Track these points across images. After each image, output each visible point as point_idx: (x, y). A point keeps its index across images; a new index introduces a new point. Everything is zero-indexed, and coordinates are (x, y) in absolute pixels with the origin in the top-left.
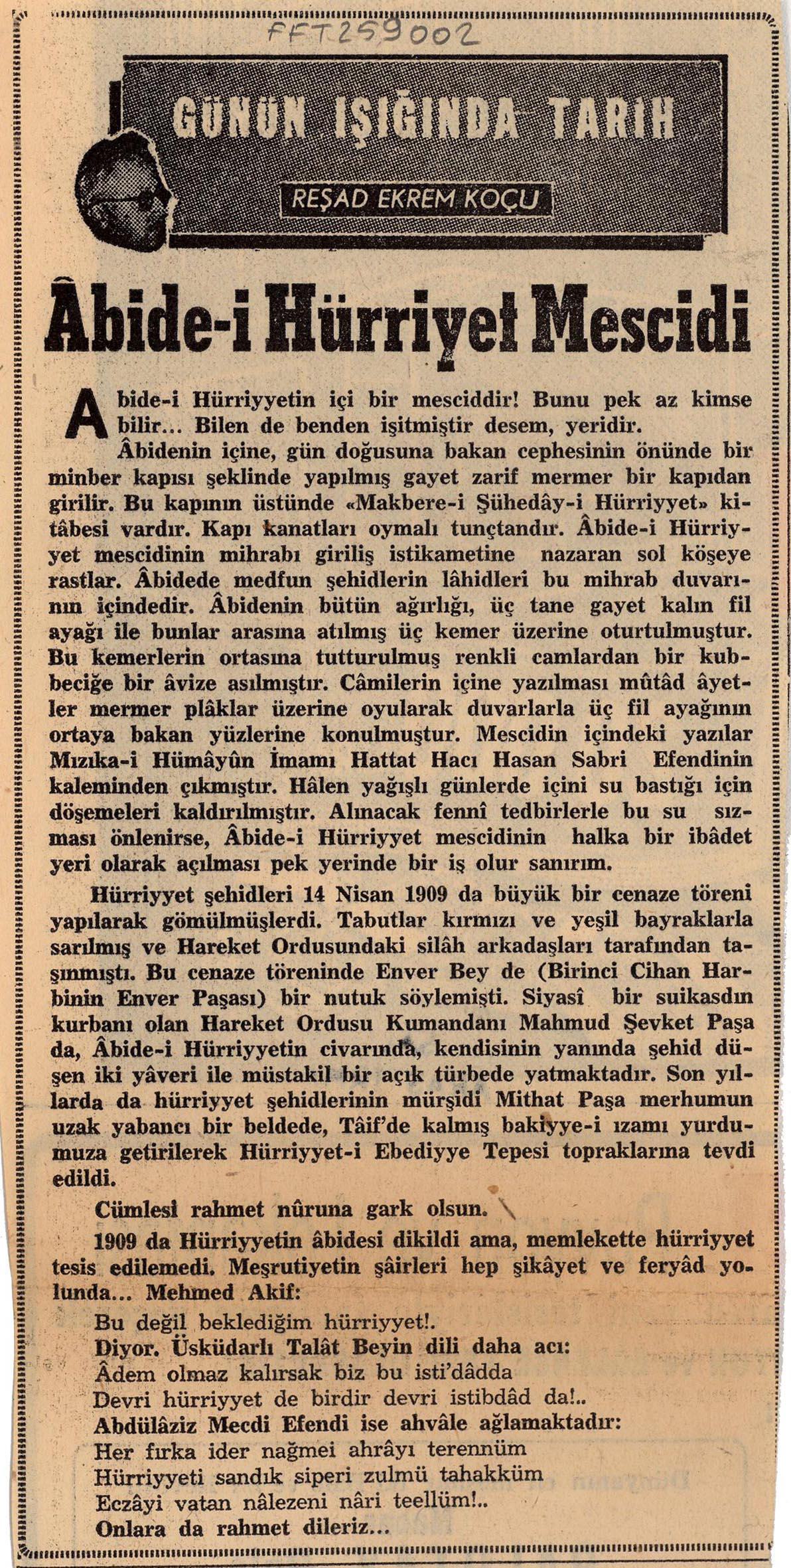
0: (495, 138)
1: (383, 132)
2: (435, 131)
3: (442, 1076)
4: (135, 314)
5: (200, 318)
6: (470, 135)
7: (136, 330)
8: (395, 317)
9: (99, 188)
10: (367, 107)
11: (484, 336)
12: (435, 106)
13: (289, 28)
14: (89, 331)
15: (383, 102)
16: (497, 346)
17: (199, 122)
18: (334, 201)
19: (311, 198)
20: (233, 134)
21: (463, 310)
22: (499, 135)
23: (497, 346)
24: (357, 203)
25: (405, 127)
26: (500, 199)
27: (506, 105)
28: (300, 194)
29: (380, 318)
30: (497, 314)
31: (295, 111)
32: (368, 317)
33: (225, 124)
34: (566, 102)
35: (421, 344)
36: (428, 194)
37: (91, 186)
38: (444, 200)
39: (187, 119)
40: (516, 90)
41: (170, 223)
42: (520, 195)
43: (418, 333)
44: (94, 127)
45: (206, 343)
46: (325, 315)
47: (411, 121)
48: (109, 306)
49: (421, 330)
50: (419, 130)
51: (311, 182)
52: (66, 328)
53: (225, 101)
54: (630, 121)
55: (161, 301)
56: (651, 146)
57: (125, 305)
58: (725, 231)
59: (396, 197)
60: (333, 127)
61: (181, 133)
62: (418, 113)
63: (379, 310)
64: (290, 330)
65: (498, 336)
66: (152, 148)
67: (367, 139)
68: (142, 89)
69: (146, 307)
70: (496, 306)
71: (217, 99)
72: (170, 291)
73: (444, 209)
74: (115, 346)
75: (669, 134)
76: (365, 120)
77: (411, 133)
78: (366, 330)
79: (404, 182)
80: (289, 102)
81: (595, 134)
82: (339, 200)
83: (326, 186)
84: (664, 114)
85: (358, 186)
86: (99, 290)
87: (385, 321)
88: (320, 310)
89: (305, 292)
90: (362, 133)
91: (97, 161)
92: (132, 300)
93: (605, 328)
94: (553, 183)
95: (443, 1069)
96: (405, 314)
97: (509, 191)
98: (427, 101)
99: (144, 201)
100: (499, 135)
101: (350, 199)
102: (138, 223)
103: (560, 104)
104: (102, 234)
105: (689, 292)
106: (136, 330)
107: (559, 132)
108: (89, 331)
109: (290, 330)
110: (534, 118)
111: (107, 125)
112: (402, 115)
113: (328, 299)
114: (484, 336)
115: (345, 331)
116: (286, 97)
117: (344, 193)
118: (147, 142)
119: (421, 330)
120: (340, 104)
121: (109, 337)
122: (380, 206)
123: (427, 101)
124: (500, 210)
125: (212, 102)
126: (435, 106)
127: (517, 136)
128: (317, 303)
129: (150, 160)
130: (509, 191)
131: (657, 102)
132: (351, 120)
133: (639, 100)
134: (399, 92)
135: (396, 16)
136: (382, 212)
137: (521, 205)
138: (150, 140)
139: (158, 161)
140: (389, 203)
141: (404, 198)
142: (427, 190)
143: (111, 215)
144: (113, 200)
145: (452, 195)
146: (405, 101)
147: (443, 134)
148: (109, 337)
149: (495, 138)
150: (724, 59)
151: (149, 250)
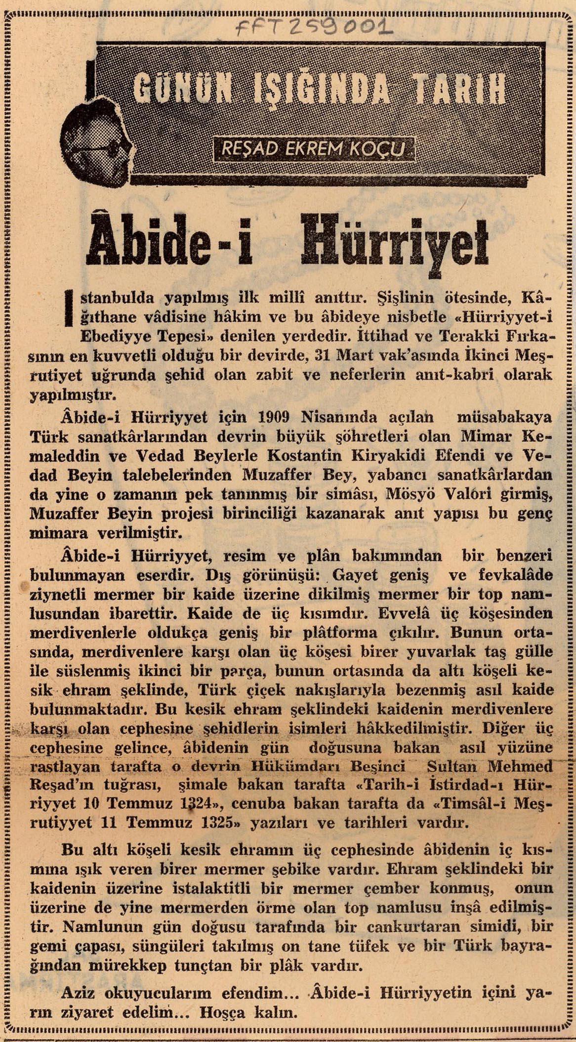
0: (373, 103)
1: (289, 99)
2: (328, 98)
3: (355, 947)
4: (154, 237)
5: (202, 239)
6: (354, 101)
7: (155, 249)
8: (398, 238)
9: (79, 141)
10: (278, 80)
11: (463, 253)
12: (328, 79)
13: (252, 23)
14: (120, 251)
15: (289, 76)
16: (473, 260)
17: (153, 92)
18: (252, 151)
19: (235, 148)
20: (178, 99)
21: (448, 234)
22: (375, 101)
23: (473, 260)
24: (271, 150)
25: (306, 96)
26: (376, 149)
27: (381, 79)
28: (228, 145)
29: (386, 240)
30: (473, 236)
31: (224, 82)
32: (378, 238)
33: (173, 93)
34: (425, 76)
35: (417, 259)
36: (323, 145)
37: (73, 138)
38: (335, 150)
39: (144, 89)
40: (256, 68)
41: (131, 166)
42: (391, 146)
43: (414, 249)
44: (76, 95)
45: (206, 259)
46: (346, 239)
47: (310, 91)
48: (134, 231)
49: (417, 246)
50: (316, 96)
51: (236, 136)
52: (102, 247)
53: (172, 76)
54: (473, 91)
55: (173, 228)
56: (487, 109)
57: (146, 229)
58: (543, 173)
59: (299, 147)
60: (253, 96)
61: (305, 101)
62: (316, 85)
63: (386, 234)
64: (320, 248)
65: (474, 252)
66: (118, 110)
67: (277, 104)
68: (110, 66)
69: (162, 231)
70: (472, 230)
71: (166, 74)
72: (180, 219)
73: (334, 157)
74: (139, 260)
75: (502, 101)
76: (276, 90)
77: (310, 100)
78: (376, 248)
79: (305, 136)
80: (220, 76)
81: (447, 100)
82: (257, 149)
83: (247, 139)
84: (498, 86)
85: (272, 139)
86: (127, 219)
87: (390, 242)
88: (342, 234)
89: (331, 220)
90: (273, 100)
91: (77, 120)
92: (152, 226)
93: (464, 247)
94: (415, 137)
95: (355, 942)
96: (405, 237)
97: (383, 143)
98: (322, 76)
99: (112, 150)
100: (375, 101)
101: (265, 147)
102: (108, 166)
103: (420, 77)
104: (81, 175)
105: (242, 220)
106: (155, 249)
107: (420, 99)
108: (120, 251)
109: (320, 248)
110: (402, 86)
111: (85, 93)
112: (304, 88)
113: (347, 225)
114: (463, 253)
115: (361, 249)
116: (217, 73)
117: (260, 144)
118: (114, 106)
119: (417, 246)
120: (258, 76)
121: (135, 254)
122: (287, 153)
123: (322, 76)
124: (376, 157)
125: (163, 76)
126: (328, 79)
127: (389, 102)
128: (340, 228)
129: (116, 120)
130: (383, 143)
131: (493, 77)
132: (265, 91)
133: (480, 75)
134: (301, 69)
135: (329, 14)
136: (288, 158)
137: (393, 153)
138: (116, 105)
139: (124, 120)
140: (294, 151)
141: (305, 148)
142: (321, 143)
143: (85, 159)
144: (89, 149)
145: (341, 145)
146: (305, 75)
147: (334, 101)
148: (135, 254)
149: (373, 103)
150: (543, 45)
151: (115, 186)
